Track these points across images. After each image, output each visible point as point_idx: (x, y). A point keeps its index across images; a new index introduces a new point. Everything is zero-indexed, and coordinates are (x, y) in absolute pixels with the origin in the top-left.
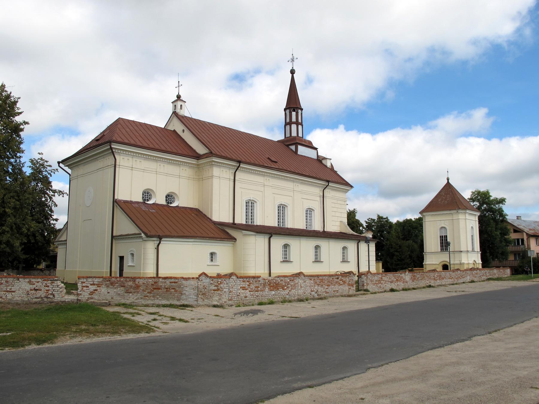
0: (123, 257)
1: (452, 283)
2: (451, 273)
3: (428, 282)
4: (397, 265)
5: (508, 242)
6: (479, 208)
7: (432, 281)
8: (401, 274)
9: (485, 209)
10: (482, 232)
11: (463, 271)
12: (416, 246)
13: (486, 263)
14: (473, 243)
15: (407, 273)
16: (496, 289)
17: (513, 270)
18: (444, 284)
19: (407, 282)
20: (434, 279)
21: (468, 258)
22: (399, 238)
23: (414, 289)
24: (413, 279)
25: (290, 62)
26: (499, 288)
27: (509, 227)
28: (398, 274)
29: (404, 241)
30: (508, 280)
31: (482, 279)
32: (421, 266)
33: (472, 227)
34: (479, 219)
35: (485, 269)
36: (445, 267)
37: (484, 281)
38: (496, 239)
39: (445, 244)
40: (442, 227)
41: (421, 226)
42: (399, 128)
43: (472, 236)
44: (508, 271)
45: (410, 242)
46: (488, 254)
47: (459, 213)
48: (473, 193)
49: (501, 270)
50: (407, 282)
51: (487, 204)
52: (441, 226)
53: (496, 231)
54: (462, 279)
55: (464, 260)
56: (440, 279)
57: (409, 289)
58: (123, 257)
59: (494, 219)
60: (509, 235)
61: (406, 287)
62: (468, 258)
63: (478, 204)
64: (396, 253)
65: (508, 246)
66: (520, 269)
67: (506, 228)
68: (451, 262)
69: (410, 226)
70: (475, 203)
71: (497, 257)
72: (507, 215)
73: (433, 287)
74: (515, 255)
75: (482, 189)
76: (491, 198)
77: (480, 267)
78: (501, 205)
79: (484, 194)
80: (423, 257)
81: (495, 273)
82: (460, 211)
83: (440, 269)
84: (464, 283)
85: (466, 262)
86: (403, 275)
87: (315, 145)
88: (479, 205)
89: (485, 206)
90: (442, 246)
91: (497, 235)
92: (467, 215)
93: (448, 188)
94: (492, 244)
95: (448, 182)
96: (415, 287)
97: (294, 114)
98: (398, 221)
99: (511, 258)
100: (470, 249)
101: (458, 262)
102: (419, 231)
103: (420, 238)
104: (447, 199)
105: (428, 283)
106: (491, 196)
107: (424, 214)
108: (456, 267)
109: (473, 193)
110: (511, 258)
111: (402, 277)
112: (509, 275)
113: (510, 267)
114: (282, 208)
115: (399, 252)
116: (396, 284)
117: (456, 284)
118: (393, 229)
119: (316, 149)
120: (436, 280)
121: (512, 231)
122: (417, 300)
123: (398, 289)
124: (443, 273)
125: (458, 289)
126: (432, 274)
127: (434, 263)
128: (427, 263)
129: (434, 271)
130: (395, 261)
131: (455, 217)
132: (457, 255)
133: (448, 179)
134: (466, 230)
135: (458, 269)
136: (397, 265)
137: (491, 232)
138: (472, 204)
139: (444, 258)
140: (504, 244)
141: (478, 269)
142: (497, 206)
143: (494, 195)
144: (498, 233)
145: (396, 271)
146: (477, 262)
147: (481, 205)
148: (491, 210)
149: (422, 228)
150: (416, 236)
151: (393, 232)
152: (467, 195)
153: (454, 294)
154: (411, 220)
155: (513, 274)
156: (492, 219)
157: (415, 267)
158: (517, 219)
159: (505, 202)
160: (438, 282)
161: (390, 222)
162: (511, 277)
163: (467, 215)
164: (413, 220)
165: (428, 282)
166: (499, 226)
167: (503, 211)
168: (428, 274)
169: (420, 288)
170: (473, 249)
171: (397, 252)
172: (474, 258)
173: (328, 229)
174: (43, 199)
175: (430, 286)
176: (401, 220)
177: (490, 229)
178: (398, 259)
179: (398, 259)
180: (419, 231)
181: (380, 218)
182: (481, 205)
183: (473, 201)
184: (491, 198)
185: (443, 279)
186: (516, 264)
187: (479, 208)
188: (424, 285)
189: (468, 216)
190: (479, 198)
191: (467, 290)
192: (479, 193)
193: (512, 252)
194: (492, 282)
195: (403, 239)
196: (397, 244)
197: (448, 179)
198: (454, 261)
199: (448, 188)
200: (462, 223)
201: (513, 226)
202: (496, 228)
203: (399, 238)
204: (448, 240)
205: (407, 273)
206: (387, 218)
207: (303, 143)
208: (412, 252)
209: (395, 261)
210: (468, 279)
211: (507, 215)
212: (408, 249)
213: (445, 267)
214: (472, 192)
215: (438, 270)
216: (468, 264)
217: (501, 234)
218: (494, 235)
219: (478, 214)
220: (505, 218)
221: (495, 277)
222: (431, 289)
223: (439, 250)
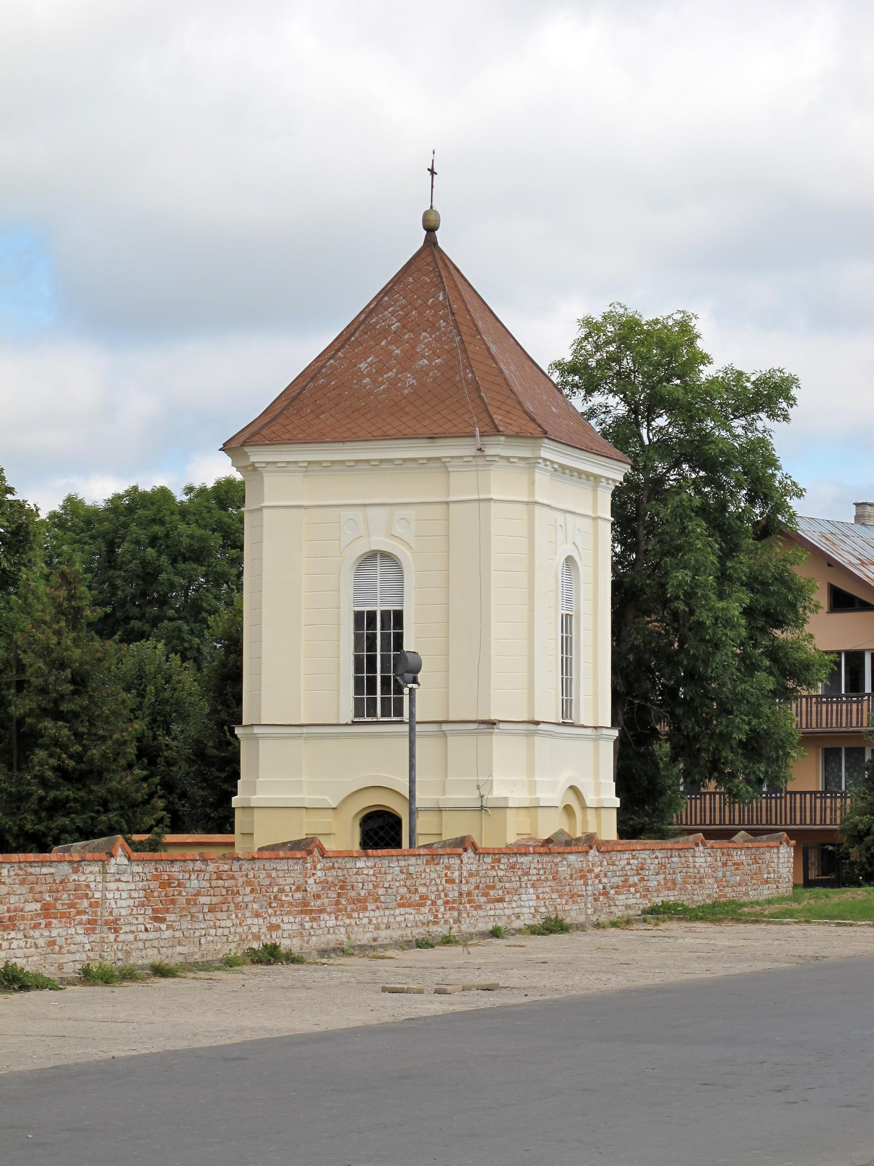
1: (419, 932)
2: (415, 865)
3: (257, 925)
4: (57, 807)
5: (790, 669)
6: (621, 437)
7: (289, 923)
8: (76, 866)
9: (663, 447)
10: (629, 599)
11: (497, 854)
12: (189, 681)
13: (643, 806)
14: (566, 666)
15: (120, 859)
16: (699, 971)
17: (814, 857)
18: (365, 938)
19: (114, 926)
20: (304, 908)
21: (530, 770)
22: (74, 617)
23: (161, 971)
24: (160, 906)
26: (719, 970)
27: (801, 572)
28: (53, 868)
29: (110, 645)
30: (778, 917)
31: (618, 912)
32: (220, 819)
33: (569, 560)
34: (617, 509)
35: (635, 843)
36: (381, 830)
37: (626, 923)
38: (717, 646)
39: (383, 668)
40: (372, 556)
41: (233, 540)
43: (567, 621)
44: (783, 859)
45: (152, 650)
46: (663, 749)
47: (491, 461)
48: (592, 328)
49: (740, 856)
50: (114, 926)
51: (671, 406)
52: (362, 548)
53: (721, 596)
54: (490, 910)
55: (507, 788)
56: (338, 910)
57: (128, 975)
59: (716, 517)
60: (799, 622)
61: (111, 958)
62: (530, 770)
63: (617, 406)
64: (48, 725)
65: (785, 694)
66: (855, 853)
67: (784, 580)
68: (422, 799)
69: (153, 541)
70: (597, 399)
71: (715, 768)
72: (799, 494)
73: (291, 959)
74: (830, 756)
75: (653, 308)
76: (707, 372)
77: (609, 830)
78: (763, 421)
79: (661, 344)
80: (235, 760)
81: (696, 866)
82: (497, 448)
83: (346, 836)
84: (495, 933)
85: (518, 796)
86: (90, 874)
88: (622, 410)
89: (662, 421)
90: (364, 685)
91: (729, 623)
92: (542, 477)
93: (429, 280)
94: (694, 677)
95: (431, 241)
96: (172, 956)
98: (72, 504)
99: (805, 774)
100: (548, 708)
101: (469, 798)
102: (217, 579)
103: (218, 623)
104: (417, 359)
105: (256, 930)
106: (705, 359)
107: (257, 456)
108: (453, 829)
109: (592, 328)
110: (805, 774)
111: (83, 892)
112: (786, 888)
113: (792, 834)
115: (70, 718)
116: (40, 936)
117: (447, 941)
118: (38, 555)
120: (315, 914)
121: (821, 597)
122: (182, 1045)
123: (49, 972)
124: (366, 866)
125: (453, 976)
126: (287, 874)
127: (307, 797)
128: (259, 798)
129: (305, 847)
130: (43, 782)
131: (462, 485)
132: (460, 746)
133: (431, 229)
134: (526, 573)
135: (463, 844)
136: (57, 807)
137: (690, 596)
138: (578, 402)
139: (374, 764)
140: (770, 683)
141: (590, 841)
142: (738, 425)
143: (728, 350)
144: (736, 611)
145: (44, 848)
146: (591, 800)
148: (699, 452)
149: (237, 561)
150: (196, 611)
151: (33, 576)
152: (548, 336)
153: (432, 1006)
154: (164, 494)
155: (808, 884)
156: (703, 511)
157: (176, 827)
158: (859, 518)
159: (791, 400)
160: (330, 929)
161: (19, 506)
162: (795, 899)
163: (542, 477)
164: (181, 497)
165: (257, 925)
166: (743, 564)
167: (772, 462)
168: (260, 873)
169: (205, 966)
170: (567, 707)
171: (57, 715)
172: (572, 772)
174: (631, 657)
175: (271, 955)
176: (98, 492)
177: (681, 575)
178: (60, 770)
179: (60, 770)
180: (217, 579)
183: (590, 389)
184: (707, 372)
185: (360, 903)
186: (834, 815)
187: (621, 437)
188: (233, 949)
189: (545, 486)
190: (627, 363)
191: (514, 978)
192: (629, 332)
193: (809, 739)
194: (675, 927)
195: (105, 628)
196: (62, 665)
197: (431, 229)
198: (439, 789)
199: (429, 280)
200: (504, 529)
201: (831, 563)
202: (723, 577)
203: (74, 617)
204: (408, 645)
205: (120, 859)
208: (160, 720)
209: (43, 782)
210: (527, 907)
211: (799, 494)
212: (130, 698)
213: (381, 830)
214: (587, 322)
215: (330, 845)
216: (533, 808)
217: (748, 612)
218: (706, 617)
219: (616, 472)
220: (780, 507)
221: (701, 897)
222: (282, 972)
223: (347, 713)
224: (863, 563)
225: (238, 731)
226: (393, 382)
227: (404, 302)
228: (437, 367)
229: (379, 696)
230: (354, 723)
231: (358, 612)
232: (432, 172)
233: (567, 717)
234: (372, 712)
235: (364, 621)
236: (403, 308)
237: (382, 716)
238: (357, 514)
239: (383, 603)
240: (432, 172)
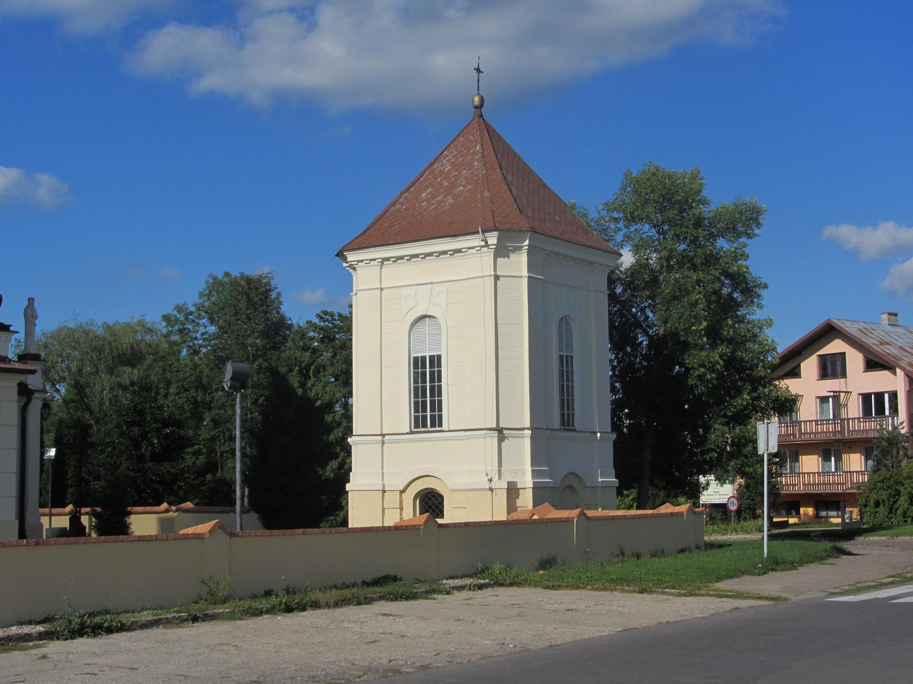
143: (717, 198)
224: (881, 344)
225: (349, 440)
226: (440, 202)
227: (456, 153)
228: (469, 190)
229: (428, 413)
230: (412, 433)
231: (834, 376)
232: (478, 70)
233: (569, 425)
234: (425, 426)
235: (418, 363)
236: (454, 156)
237: (431, 427)
238: (411, 290)
239: (430, 350)
240: (478, 70)
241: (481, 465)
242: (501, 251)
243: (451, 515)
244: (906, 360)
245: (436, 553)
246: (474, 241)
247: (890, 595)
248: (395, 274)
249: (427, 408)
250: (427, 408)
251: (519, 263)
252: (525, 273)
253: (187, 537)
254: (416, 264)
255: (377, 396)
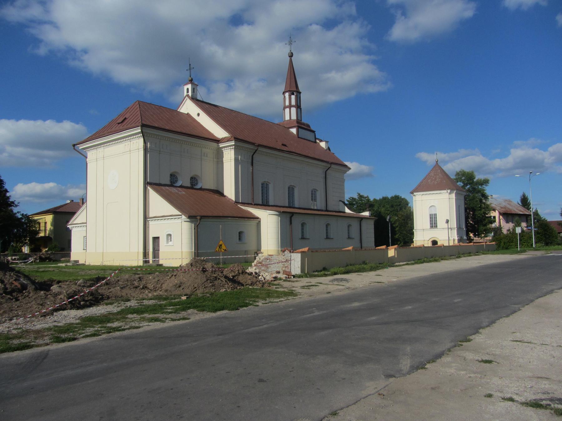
0: (158, 238)
25: (287, 45)
42: (65, 121)
58: (158, 238)
87: (312, 128)
97: (293, 97)
114: (291, 190)
119: (314, 132)
128: (417, 239)
147: (465, 185)
173: (161, 182)
181: (361, 197)
182: (465, 185)
206: (368, 197)
207: (303, 126)
241: (447, 235)
242: (450, 193)
243: (439, 244)
244: (498, 208)
245: (435, 252)
246: (445, 191)
247: (179, 322)
248: (425, 197)
249: (434, 224)
250: (434, 224)
251: (453, 196)
252: (454, 197)
253: (345, 250)
254: (430, 195)
255: (420, 222)
